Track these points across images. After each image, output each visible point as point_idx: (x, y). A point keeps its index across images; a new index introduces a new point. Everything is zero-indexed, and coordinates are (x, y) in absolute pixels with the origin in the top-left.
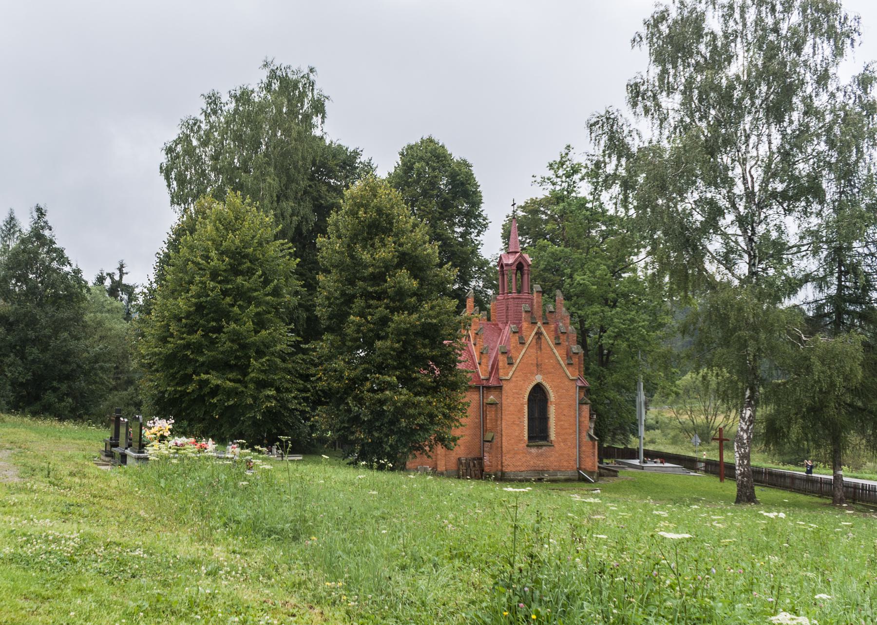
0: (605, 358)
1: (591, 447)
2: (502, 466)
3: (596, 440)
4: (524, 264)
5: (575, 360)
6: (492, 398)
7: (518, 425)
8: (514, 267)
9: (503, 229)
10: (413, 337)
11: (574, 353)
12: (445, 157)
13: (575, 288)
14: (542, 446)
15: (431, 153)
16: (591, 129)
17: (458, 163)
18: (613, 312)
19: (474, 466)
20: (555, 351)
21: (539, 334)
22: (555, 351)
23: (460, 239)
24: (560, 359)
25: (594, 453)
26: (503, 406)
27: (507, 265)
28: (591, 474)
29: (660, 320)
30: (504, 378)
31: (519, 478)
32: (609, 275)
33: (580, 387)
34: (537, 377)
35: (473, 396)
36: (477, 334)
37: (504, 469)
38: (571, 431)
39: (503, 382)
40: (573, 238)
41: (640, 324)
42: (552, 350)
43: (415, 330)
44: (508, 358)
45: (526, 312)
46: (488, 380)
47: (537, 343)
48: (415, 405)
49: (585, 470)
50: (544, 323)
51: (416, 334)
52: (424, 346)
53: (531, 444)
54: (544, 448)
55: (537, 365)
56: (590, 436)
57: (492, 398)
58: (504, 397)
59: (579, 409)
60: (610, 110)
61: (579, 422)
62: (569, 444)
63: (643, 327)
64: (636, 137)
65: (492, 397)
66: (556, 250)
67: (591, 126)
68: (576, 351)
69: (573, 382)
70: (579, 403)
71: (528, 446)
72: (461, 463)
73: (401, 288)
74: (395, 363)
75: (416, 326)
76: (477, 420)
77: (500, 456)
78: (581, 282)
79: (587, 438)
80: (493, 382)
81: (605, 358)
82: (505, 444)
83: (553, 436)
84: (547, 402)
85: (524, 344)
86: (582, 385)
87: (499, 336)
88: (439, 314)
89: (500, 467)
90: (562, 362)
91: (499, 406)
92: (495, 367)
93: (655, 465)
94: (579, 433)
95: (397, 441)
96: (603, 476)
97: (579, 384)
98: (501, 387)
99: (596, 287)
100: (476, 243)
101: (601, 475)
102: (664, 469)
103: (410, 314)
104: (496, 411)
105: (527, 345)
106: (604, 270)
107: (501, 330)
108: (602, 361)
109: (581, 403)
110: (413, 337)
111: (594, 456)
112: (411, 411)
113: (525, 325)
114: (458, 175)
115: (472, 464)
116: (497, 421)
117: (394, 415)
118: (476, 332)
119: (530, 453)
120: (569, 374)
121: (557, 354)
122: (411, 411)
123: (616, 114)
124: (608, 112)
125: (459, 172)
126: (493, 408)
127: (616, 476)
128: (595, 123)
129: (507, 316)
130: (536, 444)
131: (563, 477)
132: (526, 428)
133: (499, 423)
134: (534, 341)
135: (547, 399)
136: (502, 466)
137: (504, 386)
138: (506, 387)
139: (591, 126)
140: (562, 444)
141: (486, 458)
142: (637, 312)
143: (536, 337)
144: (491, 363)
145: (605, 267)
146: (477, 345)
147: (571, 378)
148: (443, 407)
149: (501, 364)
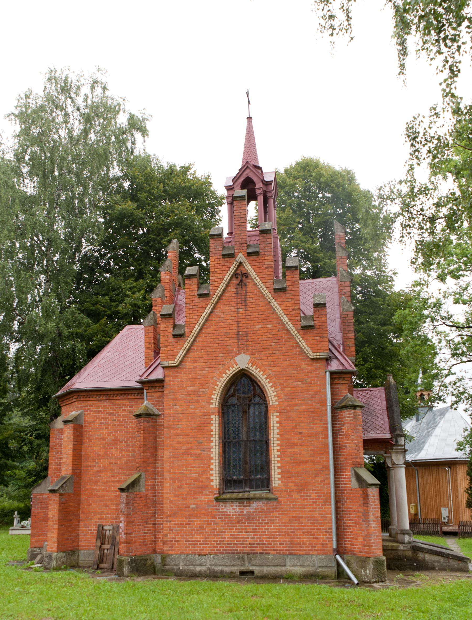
1: (361, 501)
7: (198, 456)
20: (275, 304)
22: (275, 304)
24: (285, 319)
31: (198, 569)
34: (238, 358)
38: (318, 467)
47: (237, 293)
54: (255, 504)
55: (238, 336)
62: (314, 495)
79: (354, 483)
90: (290, 326)
119: (225, 515)
131: (299, 570)
134: (232, 290)
147: (312, 354)
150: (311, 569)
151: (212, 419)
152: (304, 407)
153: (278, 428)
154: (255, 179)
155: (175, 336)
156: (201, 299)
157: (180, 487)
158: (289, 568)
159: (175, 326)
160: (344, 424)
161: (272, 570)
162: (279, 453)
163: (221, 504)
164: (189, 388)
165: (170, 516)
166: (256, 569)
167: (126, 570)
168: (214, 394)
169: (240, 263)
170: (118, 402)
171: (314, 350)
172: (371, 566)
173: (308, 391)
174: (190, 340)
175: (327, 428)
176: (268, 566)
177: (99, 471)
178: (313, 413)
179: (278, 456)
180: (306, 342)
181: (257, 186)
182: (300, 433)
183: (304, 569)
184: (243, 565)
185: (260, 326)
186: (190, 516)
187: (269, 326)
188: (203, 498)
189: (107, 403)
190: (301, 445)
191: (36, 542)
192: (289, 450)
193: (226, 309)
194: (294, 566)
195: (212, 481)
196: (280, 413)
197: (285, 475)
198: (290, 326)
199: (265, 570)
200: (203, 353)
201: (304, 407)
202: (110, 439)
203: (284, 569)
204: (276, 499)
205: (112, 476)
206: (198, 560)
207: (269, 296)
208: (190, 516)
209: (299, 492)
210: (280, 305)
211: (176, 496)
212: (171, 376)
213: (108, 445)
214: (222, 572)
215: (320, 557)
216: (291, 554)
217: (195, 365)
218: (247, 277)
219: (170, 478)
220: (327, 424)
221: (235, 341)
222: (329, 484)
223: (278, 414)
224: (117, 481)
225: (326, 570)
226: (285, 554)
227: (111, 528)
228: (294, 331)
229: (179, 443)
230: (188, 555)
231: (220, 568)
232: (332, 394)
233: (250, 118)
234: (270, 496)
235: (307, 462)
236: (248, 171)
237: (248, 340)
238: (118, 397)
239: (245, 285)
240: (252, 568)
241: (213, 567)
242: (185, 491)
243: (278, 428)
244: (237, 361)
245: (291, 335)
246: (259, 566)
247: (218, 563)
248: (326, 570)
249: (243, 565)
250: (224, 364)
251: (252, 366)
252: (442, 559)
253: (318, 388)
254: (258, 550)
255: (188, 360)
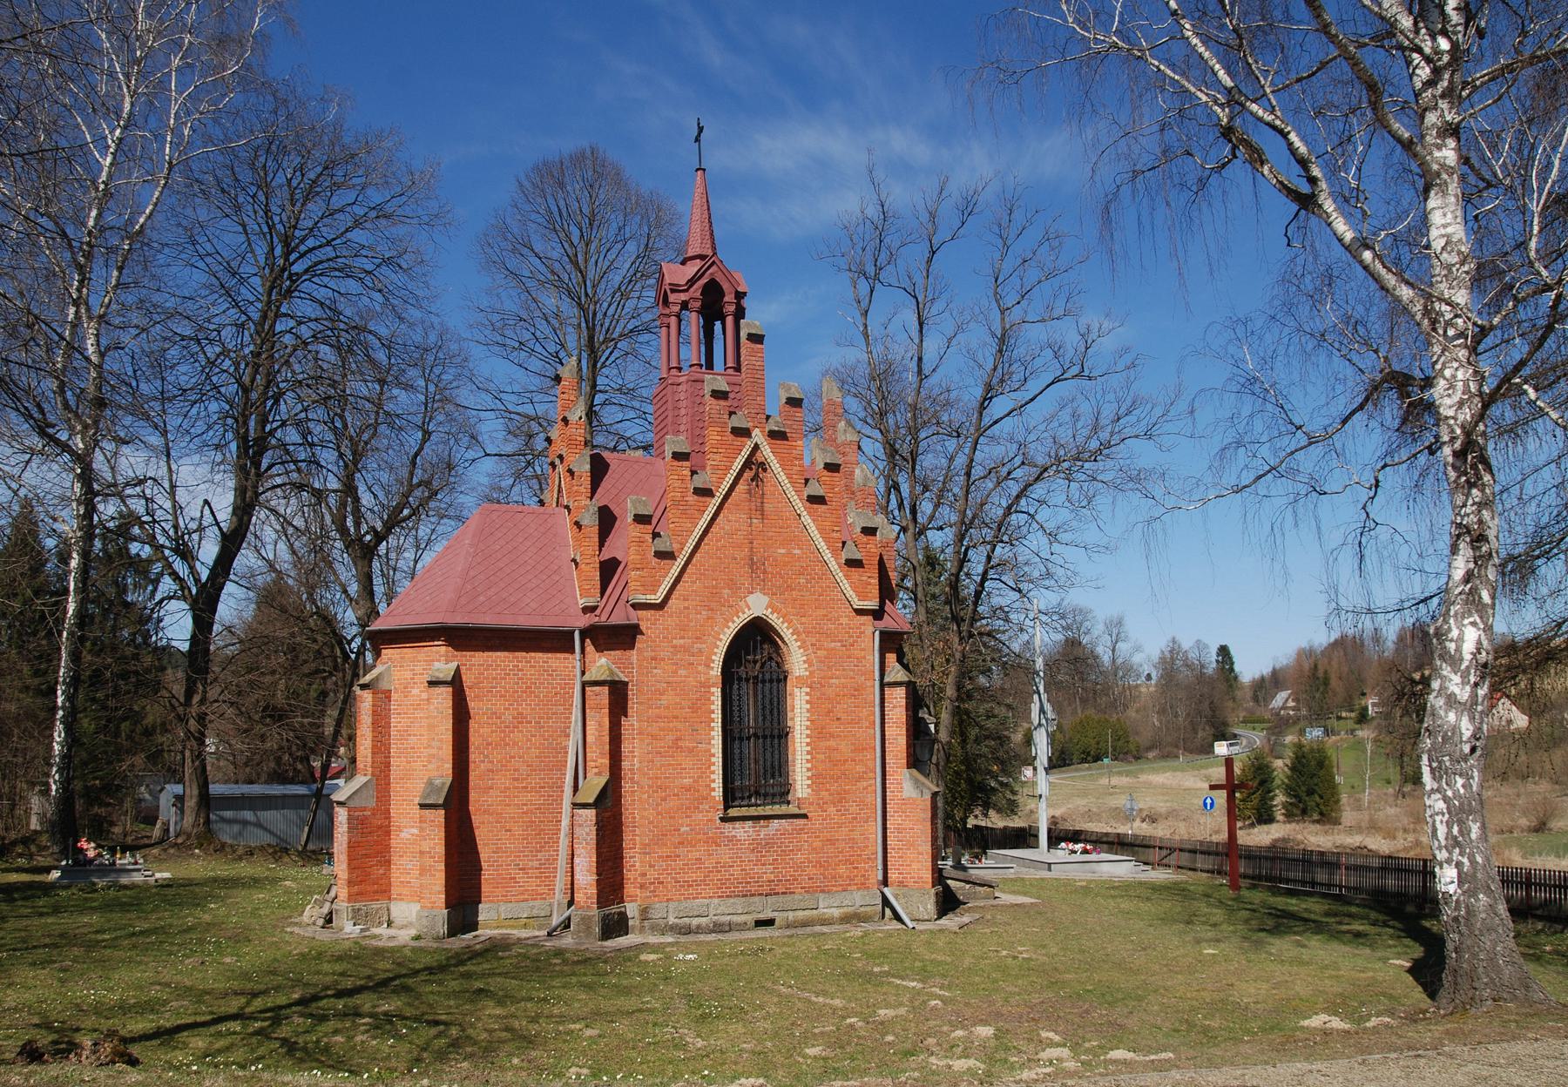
7: (691, 750)
22: (807, 519)
34: (751, 599)
55: (752, 564)
131: (836, 913)
147: (858, 604)
151: (713, 694)
154: (726, 286)
157: (664, 799)
159: (656, 535)
162: (809, 748)
168: (715, 654)
169: (756, 445)
171: (862, 597)
174: (680, 562)
181: (726, 299)
183: (842, 910)
188: (700, 816)
195: (714, 790)
197: (817, 779)
202: (508, 717)
205: (515, 779)
207: (800, 506)
210: (814, 520)
212: (648, 620)
216: (823, 891)
218: (765, 470)
228: (833, 565)
236: (714, 268)
242: (672, 803)
251: (772, 613)
254: (780, 889)
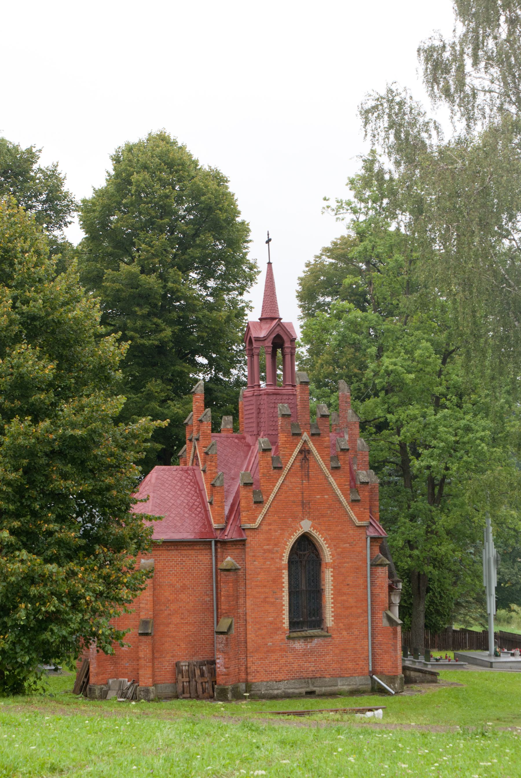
0: (436, 490)
1: (392, 636)
2: (247, 674)
3: (398, 624)
4: (285, 338)
5: (364, 495)
6: (229, 560)
7: (273, 603)
8: (269, 343)
9: (300, 284)
10: (43, 461)
11: (363, 483)
12: (183, 164)
13: (383, 377)
14: (312, 637)
15: (160, 157)
16: (367, 118)
17: (207, 175)
18: (438, 416)
19: (202, 675)
20: (331, 479)
21: (305, 452)
22: (331, 479)
23: (211, 299)
24: (339, 492)
25: (395, 646)
26: (249, 572)
27: (258, 339)
28: (391, 680)
29: (508, 428)
30: (248, 526)
31: (276, 692)
32: (433, 356)
33: (371, 538)
34: (303, 523)
35: (200, 557)
36: (207, 453)
37: (250, 678)
38: (359, 611)
39: (248, 533)
40: (385, 299)
41: (479, 435)
42: (326, 478)
43: (48, 449)
44: (254, 493)
45: (283, 416)
46: (223, 530)
47: (301, 466)
48: (44, 579)
49: (381, 675)
50: (313, 435)
51: (52, 454)
52: (65, 476)
53: (295, 635)
54: (316, 641)
55: (303, 504)
56: (390, 619)
57: (229, 560)
58: (248, 559)
59: (371, 574)
60: (394, 90)
61: (372, 594)
62: (356, 632)
63: (482, 439)
64: (434, 133)
65: (229, 558)
66: (356, 317)
67: (366, 114)
68: (366, 480)
69: (361, 531)
70: (371, 565)
71: (289, 638)
72: (181, 672)
73: (21, 376)
74: (11, 507)
75: (50, 443)
76: (208, 599)
77: (243, 656)
78: (391, 367)
79: (385, 622)
80: (231, 534)
81: (436, 490)
82: (251, 636)
83: (329, 620)
84: (320, 564)
85: (280, 468)
86: (375, 535)
87: (246, 457)
88: (88, 421)
89: (243, 675)
90: (342, 498)
91: (240, 573)
92: (235, 509)
93: (512, 659)
94: (373, 613)
95: (14, 643)
96: (414, 682)
97: (371, 533)
98: (244, 541)
99: (412, 376)
100: (241, 305)
101: (408, 681)
102: (509, 665)
103: (35, 421)
104: (236, 581)
105: (285, 471)
106: (427, 349)
107: (249, 446)
108: (433, 494)
109: (374, 565)
110: (43, 461)
111: (395, 650)
112: (33, 591)
113: (282, 438)
114: (204, 194)
115: (198, 672)
116: (237, 598)
117: (7, 597)
118: (205, 450)
119: (293, 649)
120: (354, 517)
121: (335, 485)
122: (33, 591)
123: (403, 95)
124: (390, 91)
125: (205, 190)
126: (231, 576)
127: (435, 681)
128: (373, 108)
129: (258, 423)
130: (303, 634)
131: (346, 688)
132: (286, 608)
133: (241, 601)
134: (298, 464)
135: (321, 560)
136: (247, 674)
137: (249, 539)
138: (252, 540)
139: (366, 114)
140: (345, 633)
141: (220, 662)
142: (475, 415)
143: (301, 457)
144: (230, 500)
145: (429, 344)
146: (208, 472)
147: (358, 523)
148: (95, 581)
149: (243, 504)
150: (354, 687)
152: (350, 564)
153: (332, 581)
155: (256, 503)
156: (275, 471)
157: (259, 629)
158: (340, 687)
160: (378, 577)
161: (329, 689)
163: (291, 641)
164: (266, 547)
165: (252, 652)
166: (317, 690)
167: (229, 695)
169: (305, 441)
170: (185, 552)
171: (360, 519)
172: (399, 681)
173: (354, 551)
175: (367, 581)
176: (325, 687)
177: (169, 614)
178: (357, 569)
179: (332, 603)
180: (354, 512)
182: (348, 585)
184: (308, 687)
185: (319, 497)
186: (268, 651)
187: (326, 497)
188: (277, 637)
189: (174, 552)
190: (348, 594)
191: (102, 679)
192: (339, 598)
193: (293, 480)
194: (343, 685)
196: (333, 568)
197: (337, 617)
198: (342, 498)
199: (323, 689)
200: (276, 517)
201: (350, 564)
202: (178, 586)
203: (336, 688)
204: (330, 636)
206: (276, 685)
208: (268, 651)
209: (345, 629)
210: (335, 480)
211: (257, 636)
213: (177, 591)
214: (293, 693)
215: (360, 677)
216: (340, 677)
217: (270, 527)
219: (252, 622)
220: (367, 578)
221: (300, 508)
222: (368, 623)
223: (332, 570)
224: (187, 623)
225: (364, 686)
226: (336, 677)
227: (187, 664)
229: (258, 593)
230: (267, 682)
231: (291, 691)
232: (371, 553)
233: (269, 264)
234: (326, 634)
235: (352, 607)
237: (310, 508)
238: (185, 548)
239: (308, 460)
240: (315, 689)
241: (286, 690)
243: (332, 581)
244: (302, 525)
245: (342, 505)
246: (320, 687)
247: (291, 687)
248: (364, 686)
249: (308, 687)
250: (292, 527)
252: (421, 674)
253: (361, 549)
254: (318, 675)
255: (265, 522)
